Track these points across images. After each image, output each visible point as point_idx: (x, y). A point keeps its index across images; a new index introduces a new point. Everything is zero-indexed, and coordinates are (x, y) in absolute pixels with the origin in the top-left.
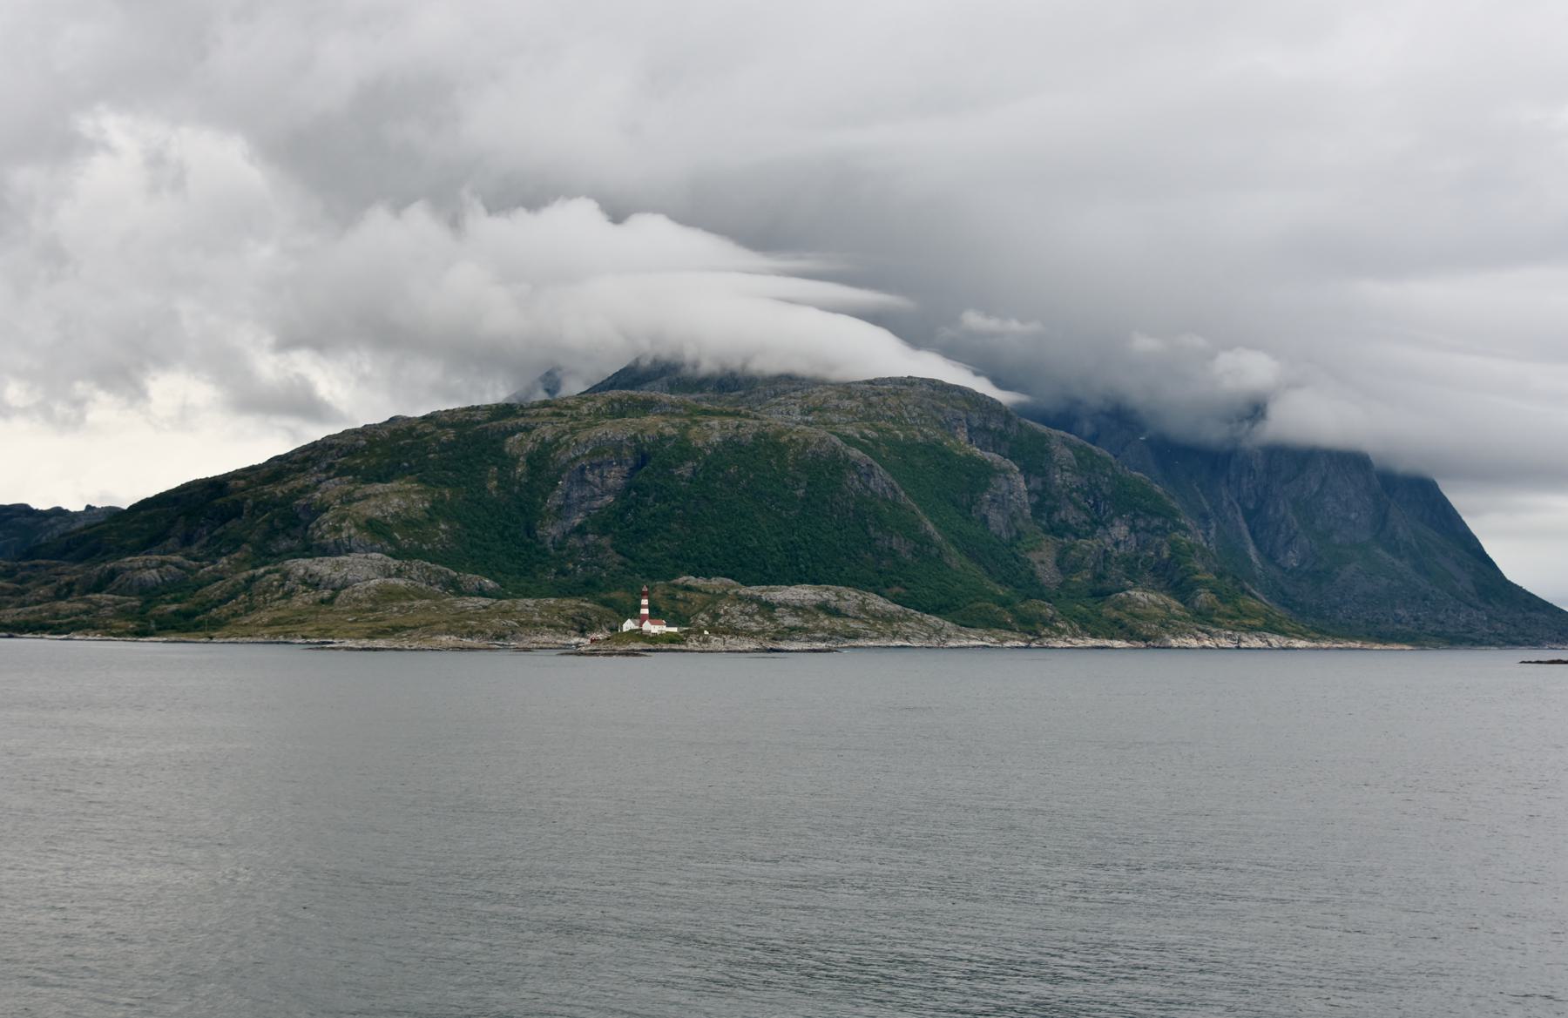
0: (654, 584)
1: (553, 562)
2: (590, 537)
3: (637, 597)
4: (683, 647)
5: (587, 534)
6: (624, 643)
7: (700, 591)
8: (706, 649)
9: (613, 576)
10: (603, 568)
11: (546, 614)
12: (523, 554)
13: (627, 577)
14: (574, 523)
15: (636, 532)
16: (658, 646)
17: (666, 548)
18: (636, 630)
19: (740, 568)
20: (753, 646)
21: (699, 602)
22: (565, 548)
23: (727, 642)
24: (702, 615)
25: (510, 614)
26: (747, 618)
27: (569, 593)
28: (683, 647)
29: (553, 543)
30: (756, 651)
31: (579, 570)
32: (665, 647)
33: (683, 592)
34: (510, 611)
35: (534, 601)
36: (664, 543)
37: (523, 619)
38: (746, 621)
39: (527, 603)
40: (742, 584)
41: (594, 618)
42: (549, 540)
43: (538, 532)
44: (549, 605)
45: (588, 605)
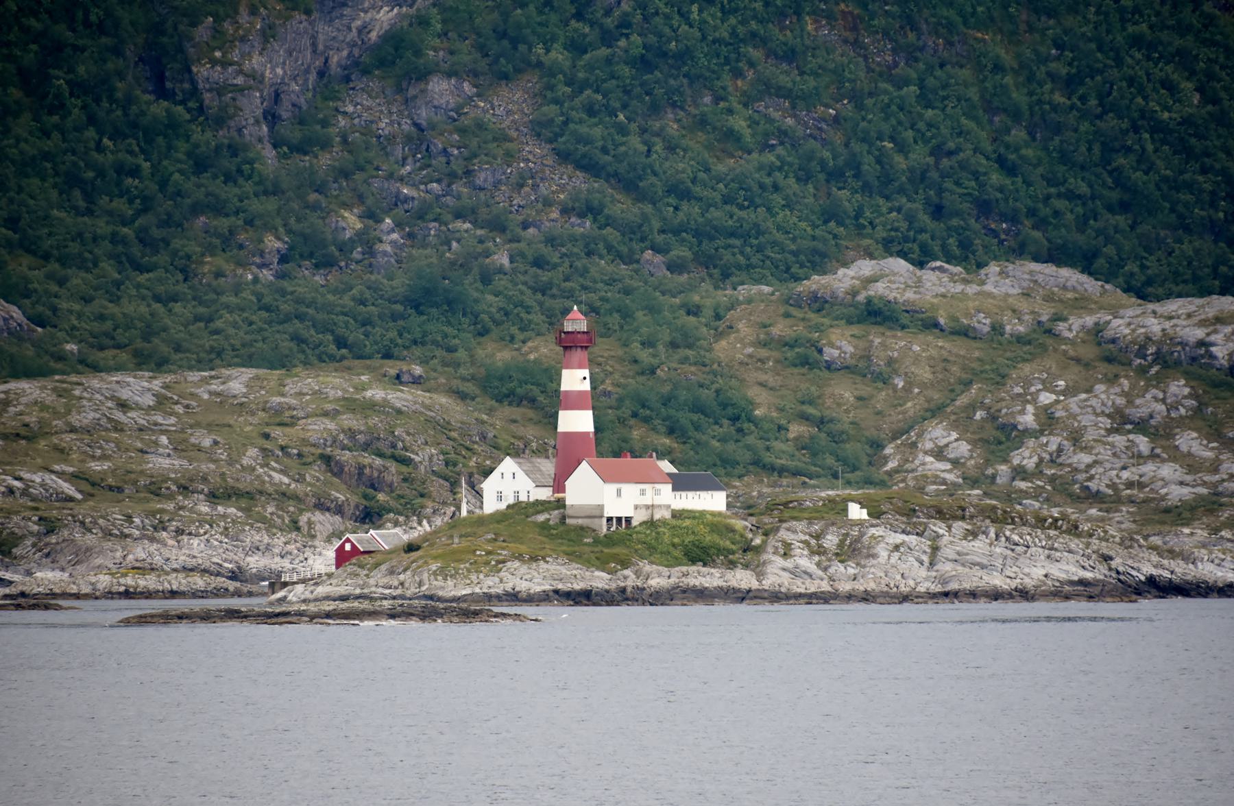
0: (723, 296)
1: (271, 204)
2: (440, 89)
3: (644, 355)
4: (742, 579)
5: (423, 75)
6: (476, 566)
7: (931, 325)
8: (845, 587)
9: (539, 263)
10: (498, 226)
11: (207, 442)
12: (135, 172)
13: (602, 265)
14: (364, 29)
15: (643, 64)
16: (629, 578)
17: (783, 134)
18: (540, 506)
19: (1121, 220)
20: (1068, 569)
21: (925, 374)
22: (325, 145)
23: (948, 552)
24: (939, 433)
25: (42, 444)
26: (1143, 443)
27: (341, 343)
28: (742, 579)
29: (271, 117)
30: (1087, 590)
31: (389, 236)
32: (659, 578)
33: (856, 330)
34: (43, 431)
35: (157, 384)
36: (777, 113)
37: (96, 466)
38: (1140, 458)
39: (125, 394)
40: (1127, 290)
41: (425, 456)
42: (253, 105)
43: (202, 71)
44: (222, 399)
45: (401, 397)
